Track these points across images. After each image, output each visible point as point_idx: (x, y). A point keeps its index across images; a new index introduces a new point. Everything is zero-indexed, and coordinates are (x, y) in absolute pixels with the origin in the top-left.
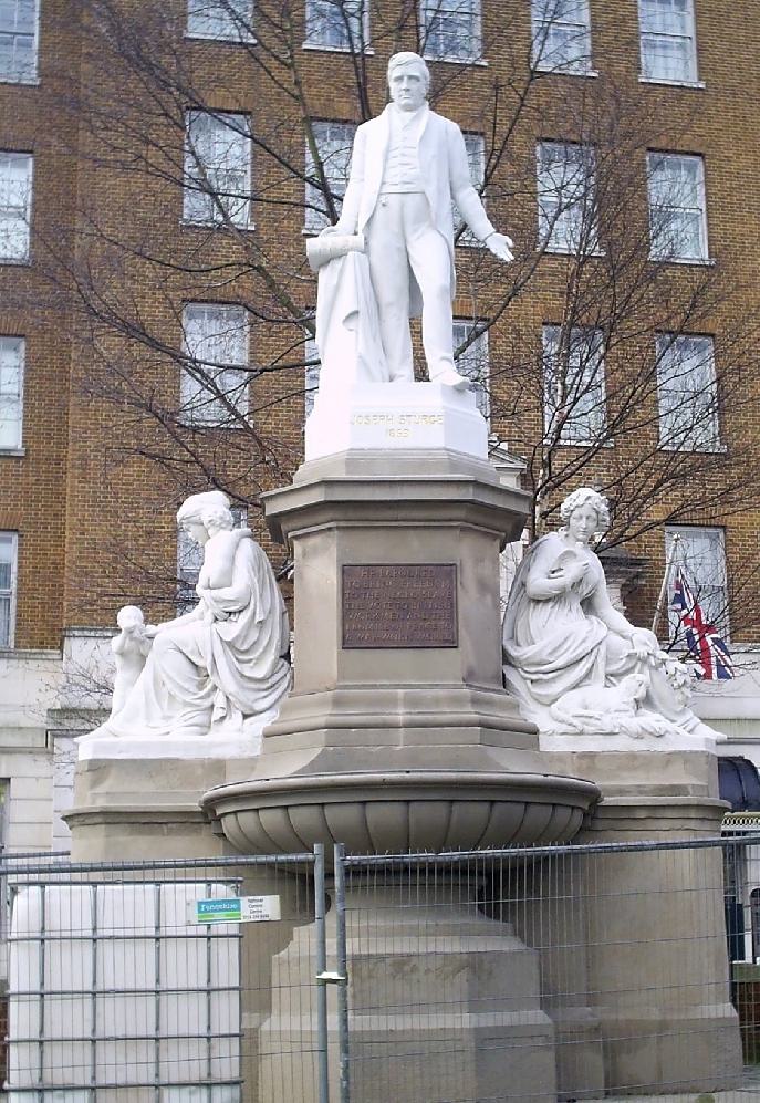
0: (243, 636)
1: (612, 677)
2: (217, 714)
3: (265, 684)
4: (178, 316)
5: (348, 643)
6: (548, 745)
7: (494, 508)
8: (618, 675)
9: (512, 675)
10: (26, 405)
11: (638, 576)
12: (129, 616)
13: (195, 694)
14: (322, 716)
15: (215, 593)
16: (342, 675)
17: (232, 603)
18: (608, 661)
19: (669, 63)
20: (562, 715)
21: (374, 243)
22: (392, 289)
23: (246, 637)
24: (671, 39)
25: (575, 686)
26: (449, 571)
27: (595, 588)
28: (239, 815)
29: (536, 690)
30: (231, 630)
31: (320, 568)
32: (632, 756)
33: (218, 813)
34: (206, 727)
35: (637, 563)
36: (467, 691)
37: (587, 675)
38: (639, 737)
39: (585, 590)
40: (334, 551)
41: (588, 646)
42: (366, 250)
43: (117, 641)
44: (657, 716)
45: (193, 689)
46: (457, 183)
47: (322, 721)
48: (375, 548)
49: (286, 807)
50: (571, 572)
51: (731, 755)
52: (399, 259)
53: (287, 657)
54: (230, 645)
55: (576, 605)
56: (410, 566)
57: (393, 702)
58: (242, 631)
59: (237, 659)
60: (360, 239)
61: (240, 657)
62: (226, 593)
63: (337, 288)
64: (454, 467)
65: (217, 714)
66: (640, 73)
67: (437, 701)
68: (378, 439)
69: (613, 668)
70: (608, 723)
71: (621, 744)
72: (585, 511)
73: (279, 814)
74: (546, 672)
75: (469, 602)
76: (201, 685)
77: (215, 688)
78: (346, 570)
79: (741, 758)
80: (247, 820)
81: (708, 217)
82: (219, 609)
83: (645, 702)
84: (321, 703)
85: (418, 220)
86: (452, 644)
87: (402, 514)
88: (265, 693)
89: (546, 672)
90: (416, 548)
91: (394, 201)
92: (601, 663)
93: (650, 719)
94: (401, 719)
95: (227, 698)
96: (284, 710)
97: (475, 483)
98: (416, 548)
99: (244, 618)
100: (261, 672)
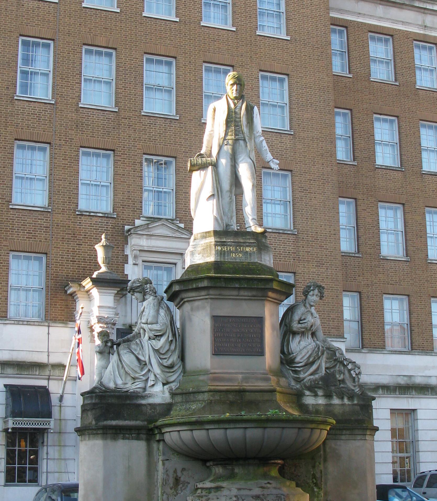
13: (139, 373)
15: (149, 326)
17: (158, 332)
19: (272, 27)
23: (164, 347)
24: (264, 11)
28: (171, 433)
33: (163, 431)
40: (208, 309)
49: (179, 431)
51: (33, 385)
58: (163, 345)
59: (160, 358)
61: (161, 357)
62: (155, 327)
66: (202, 21)
73: (189, 433)
77: (149, 370)
78: (215, 319)
81: (290, 108)
88: (172, 374)
95: (155, 375)
99: (163, 340)
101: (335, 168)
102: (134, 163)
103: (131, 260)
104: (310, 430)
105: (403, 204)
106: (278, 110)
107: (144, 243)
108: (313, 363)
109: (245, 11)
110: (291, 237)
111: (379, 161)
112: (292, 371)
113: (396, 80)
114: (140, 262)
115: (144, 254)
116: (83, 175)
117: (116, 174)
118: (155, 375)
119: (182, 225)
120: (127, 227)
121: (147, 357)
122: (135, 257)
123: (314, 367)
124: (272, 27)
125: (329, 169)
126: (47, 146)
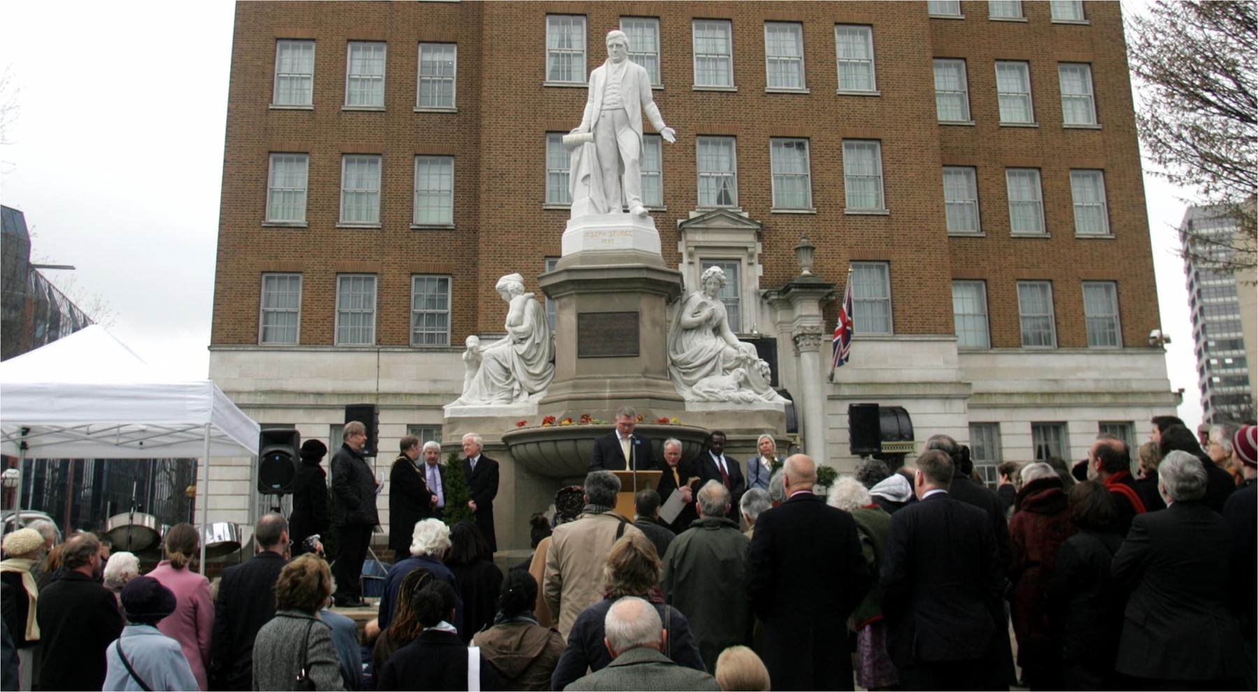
0: (528, 352)
1: (726, 370)
2: (516, 393)
3: (538, 377)
4: (543, 142)
5: (582, 354)
6: (689, 408)
7: (659, 281)
8: (730, 369)
9: (673, 371)
10: (455, 197)
11: (831, 294)
12: (471, 341)
14: (566, 393)
16: (578, 371)
18: (724, 362)
20: (700, 392)
21: (599, 137)
22: (609, 162)
25: (707, 375)
26: (635, 315)
27: (721, 321)
29: (685, 378)
30: (523, 348)
31: (568, 319)
32: (735, 413)
34: (510, 400)
35: (828, 286)
36: (643, 380)
37: (713, 370)
38: (738, 403)
39: (714, 323)
41: (713, 354)
42: (594, 140)
43: (464, 354)
44: (751, 391)
45: (503, 379)
46: (645, 101)
47: (566, 396)
48: (595, 305)
50: (705, 313)
52: (611, 144)
53: (553, 362)
54: (521, 357)
55: (709, 331)
56: (617, 310)
57: (604, 386)
60: (591, 135)
62: (520, 329)
63: (579, 163)
64: (638, 259)
65: (516, 393)
67: (627, 385)
68: (598, 245)
69: (728, 365)
70: (723, 395)
71: (729, 407)
72: (713, 279)
73: (552, 444)
74: (688, 368)
75: (646, 332)
76: (507, 378)
78: (580, 316)
79: (901, 408)
80: (521, 448)
82: (515, 338)
83: (744, 383)
84: (567, 387)
85: (621, 124)
86: (636, 353)
87: (617, 285)
89: (688, 368)
90: (617, 304)
91: (609, 114)
92: (720, 363)
93: (748, 393)
94: (607, 395)
96: (549, 391)
97: (648, 269)
98: (617, 304)
99: (528, 343)
100: (537, 371)
101: (937, 131)
102: (686, 148)
103: (685, 259)
105: (1102, 170)
106: (865, 68)
107: (700, 238)
110: (882, 220)
111: (1069, 121)
113: (1024, 15)
114: (697, 260)
115: (699, 251)
116: (775, 169)
117: (665, 161)
119: (746, 215)
120: (679, 221)
122: (691, 255)
125: (928, 133)
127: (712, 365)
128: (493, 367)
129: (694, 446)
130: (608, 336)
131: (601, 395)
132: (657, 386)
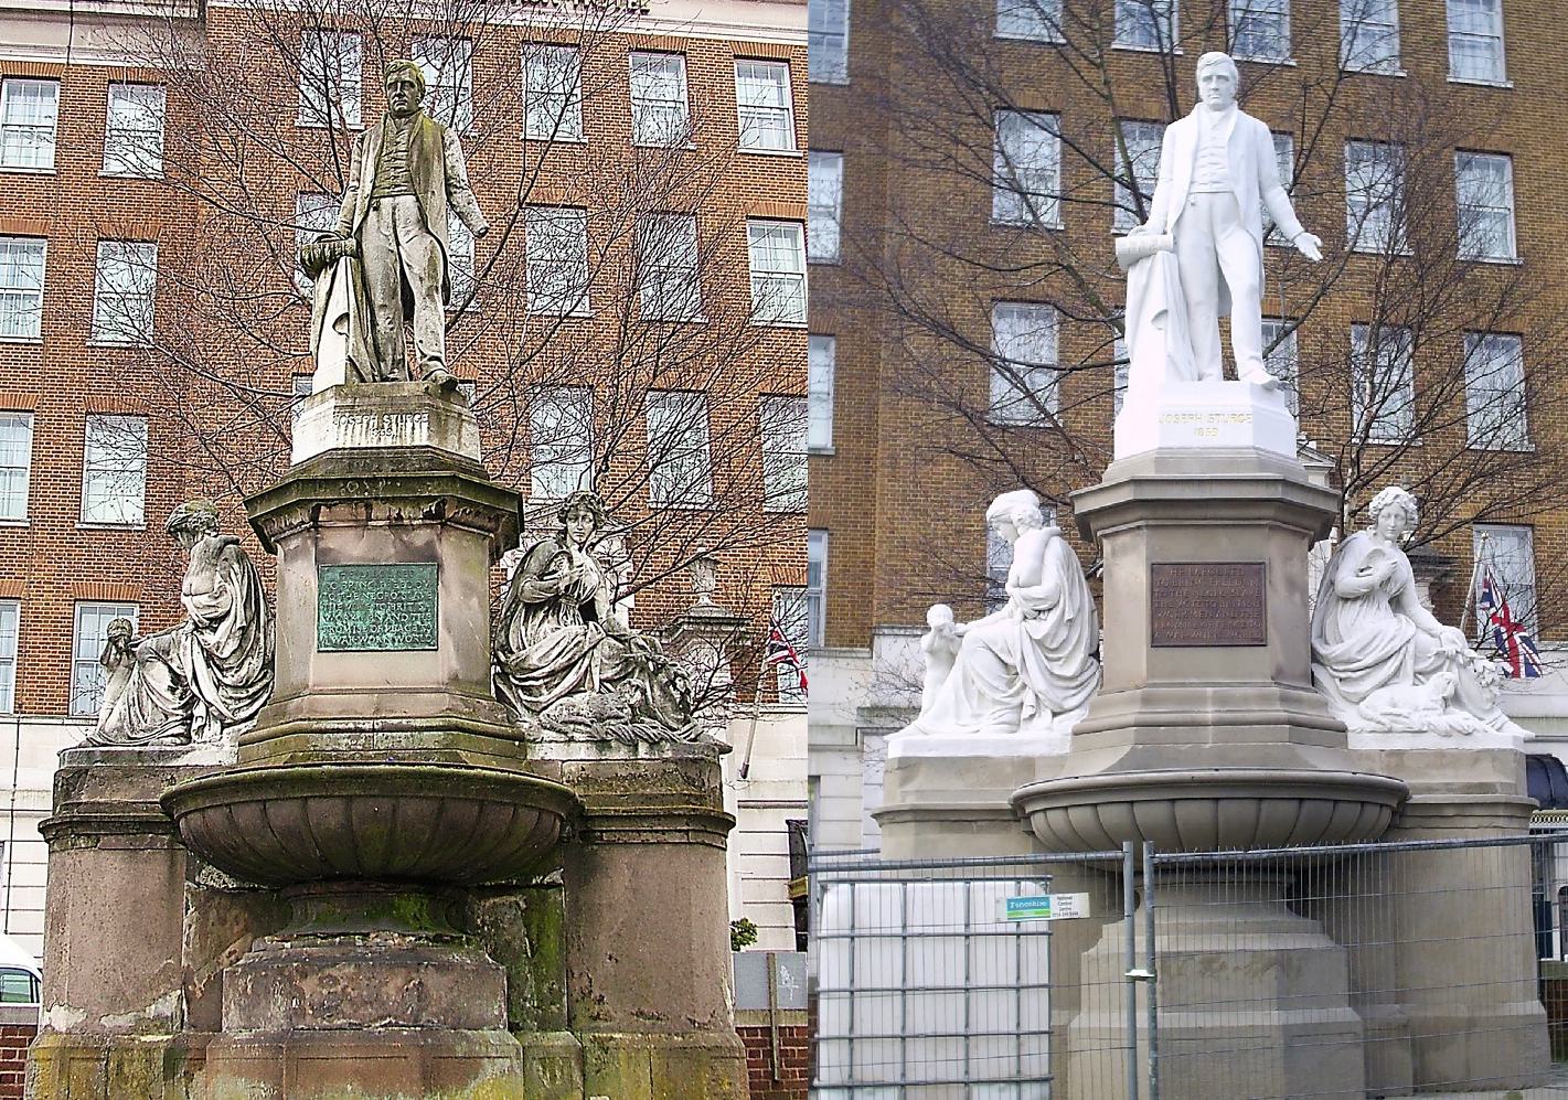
0: (1053, 634)
2: (1027, 712)
3: (1075, 682)
4: (987, 315)
5: (1157, 641)
6: (1356, 743)
7: (1303, 507)
10: (836, 404)
11: (1446, 574)
12: (939, 614)
14: (1130, 714)
16: (1151, 674)
18: (1416, 660)
21: (1184, 243)
24: (1479, 39)
25: (1384, 685)
26: (1258, 569)
28: (1048, 813)
29: (1345, 688)
30: (1040, 628)
34: (1015, 725)
35: (1445, 561)
36: (1276, 689)
38: (1447, 735)
39: (1393, 589)
41: (1396, 644)
42: (1175, 250)
43: (926, 639)
44: (1466, 714)
46: (1265, 184)
47: (1131, 719)
48: (1184, 547)
49: (1095, 805)
52: (1208, 259)
53: (1096, 655)
54: (1039, 643)
55: (1385, 603)
59: (1046, 657)
60: (1169, 237)
61: (1050, 656)
63: (1146, 287)
65: (1027, 712)
68: (1186, 438)
69: (1421, 666)
70: (1416, 721)
71: (1430, 742)
72: (1394, 509)
73: (1088, 812)
75: (1277, 601)
76: (1010, 684)
78: (1155, 569)
79: (1549, 756)
81: (1516, 216)
82: (1028, 608)
84: (1130, 701)
85: (1226, 220)
86: (1261, 642)
88: (1074, 692)
91: (1202, 200)
92: (1409, 662)
93: (1458, 717)
94: (1210, 717)
95: (1036, 696)
96: (1093, 709)
97: (1284, 482)
99: (1053, 616)
100: (1070, 671)
104: (1360, 805)
108: (569, 667)
109: (1425, 32)
112: (523, 688)
118: (1036, 696)
121: (1019, 657)
123: (572, 678)
124: (1477, 63)
126: (1516, 339)
127: (1390, 665)
128: (983, 666)
129: (548, 819)
130: (1207, 610)
131: (1199, 717)
132: (1298, 701)
